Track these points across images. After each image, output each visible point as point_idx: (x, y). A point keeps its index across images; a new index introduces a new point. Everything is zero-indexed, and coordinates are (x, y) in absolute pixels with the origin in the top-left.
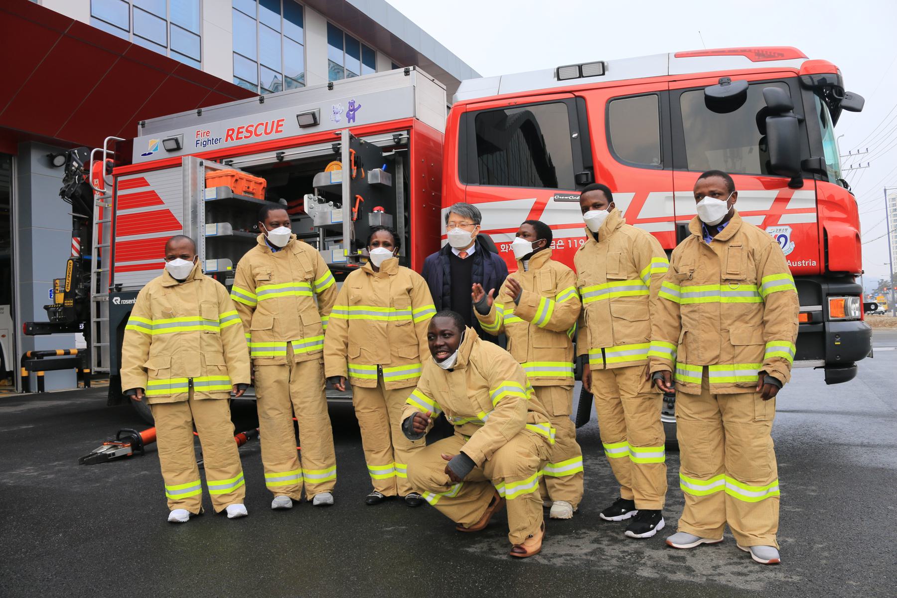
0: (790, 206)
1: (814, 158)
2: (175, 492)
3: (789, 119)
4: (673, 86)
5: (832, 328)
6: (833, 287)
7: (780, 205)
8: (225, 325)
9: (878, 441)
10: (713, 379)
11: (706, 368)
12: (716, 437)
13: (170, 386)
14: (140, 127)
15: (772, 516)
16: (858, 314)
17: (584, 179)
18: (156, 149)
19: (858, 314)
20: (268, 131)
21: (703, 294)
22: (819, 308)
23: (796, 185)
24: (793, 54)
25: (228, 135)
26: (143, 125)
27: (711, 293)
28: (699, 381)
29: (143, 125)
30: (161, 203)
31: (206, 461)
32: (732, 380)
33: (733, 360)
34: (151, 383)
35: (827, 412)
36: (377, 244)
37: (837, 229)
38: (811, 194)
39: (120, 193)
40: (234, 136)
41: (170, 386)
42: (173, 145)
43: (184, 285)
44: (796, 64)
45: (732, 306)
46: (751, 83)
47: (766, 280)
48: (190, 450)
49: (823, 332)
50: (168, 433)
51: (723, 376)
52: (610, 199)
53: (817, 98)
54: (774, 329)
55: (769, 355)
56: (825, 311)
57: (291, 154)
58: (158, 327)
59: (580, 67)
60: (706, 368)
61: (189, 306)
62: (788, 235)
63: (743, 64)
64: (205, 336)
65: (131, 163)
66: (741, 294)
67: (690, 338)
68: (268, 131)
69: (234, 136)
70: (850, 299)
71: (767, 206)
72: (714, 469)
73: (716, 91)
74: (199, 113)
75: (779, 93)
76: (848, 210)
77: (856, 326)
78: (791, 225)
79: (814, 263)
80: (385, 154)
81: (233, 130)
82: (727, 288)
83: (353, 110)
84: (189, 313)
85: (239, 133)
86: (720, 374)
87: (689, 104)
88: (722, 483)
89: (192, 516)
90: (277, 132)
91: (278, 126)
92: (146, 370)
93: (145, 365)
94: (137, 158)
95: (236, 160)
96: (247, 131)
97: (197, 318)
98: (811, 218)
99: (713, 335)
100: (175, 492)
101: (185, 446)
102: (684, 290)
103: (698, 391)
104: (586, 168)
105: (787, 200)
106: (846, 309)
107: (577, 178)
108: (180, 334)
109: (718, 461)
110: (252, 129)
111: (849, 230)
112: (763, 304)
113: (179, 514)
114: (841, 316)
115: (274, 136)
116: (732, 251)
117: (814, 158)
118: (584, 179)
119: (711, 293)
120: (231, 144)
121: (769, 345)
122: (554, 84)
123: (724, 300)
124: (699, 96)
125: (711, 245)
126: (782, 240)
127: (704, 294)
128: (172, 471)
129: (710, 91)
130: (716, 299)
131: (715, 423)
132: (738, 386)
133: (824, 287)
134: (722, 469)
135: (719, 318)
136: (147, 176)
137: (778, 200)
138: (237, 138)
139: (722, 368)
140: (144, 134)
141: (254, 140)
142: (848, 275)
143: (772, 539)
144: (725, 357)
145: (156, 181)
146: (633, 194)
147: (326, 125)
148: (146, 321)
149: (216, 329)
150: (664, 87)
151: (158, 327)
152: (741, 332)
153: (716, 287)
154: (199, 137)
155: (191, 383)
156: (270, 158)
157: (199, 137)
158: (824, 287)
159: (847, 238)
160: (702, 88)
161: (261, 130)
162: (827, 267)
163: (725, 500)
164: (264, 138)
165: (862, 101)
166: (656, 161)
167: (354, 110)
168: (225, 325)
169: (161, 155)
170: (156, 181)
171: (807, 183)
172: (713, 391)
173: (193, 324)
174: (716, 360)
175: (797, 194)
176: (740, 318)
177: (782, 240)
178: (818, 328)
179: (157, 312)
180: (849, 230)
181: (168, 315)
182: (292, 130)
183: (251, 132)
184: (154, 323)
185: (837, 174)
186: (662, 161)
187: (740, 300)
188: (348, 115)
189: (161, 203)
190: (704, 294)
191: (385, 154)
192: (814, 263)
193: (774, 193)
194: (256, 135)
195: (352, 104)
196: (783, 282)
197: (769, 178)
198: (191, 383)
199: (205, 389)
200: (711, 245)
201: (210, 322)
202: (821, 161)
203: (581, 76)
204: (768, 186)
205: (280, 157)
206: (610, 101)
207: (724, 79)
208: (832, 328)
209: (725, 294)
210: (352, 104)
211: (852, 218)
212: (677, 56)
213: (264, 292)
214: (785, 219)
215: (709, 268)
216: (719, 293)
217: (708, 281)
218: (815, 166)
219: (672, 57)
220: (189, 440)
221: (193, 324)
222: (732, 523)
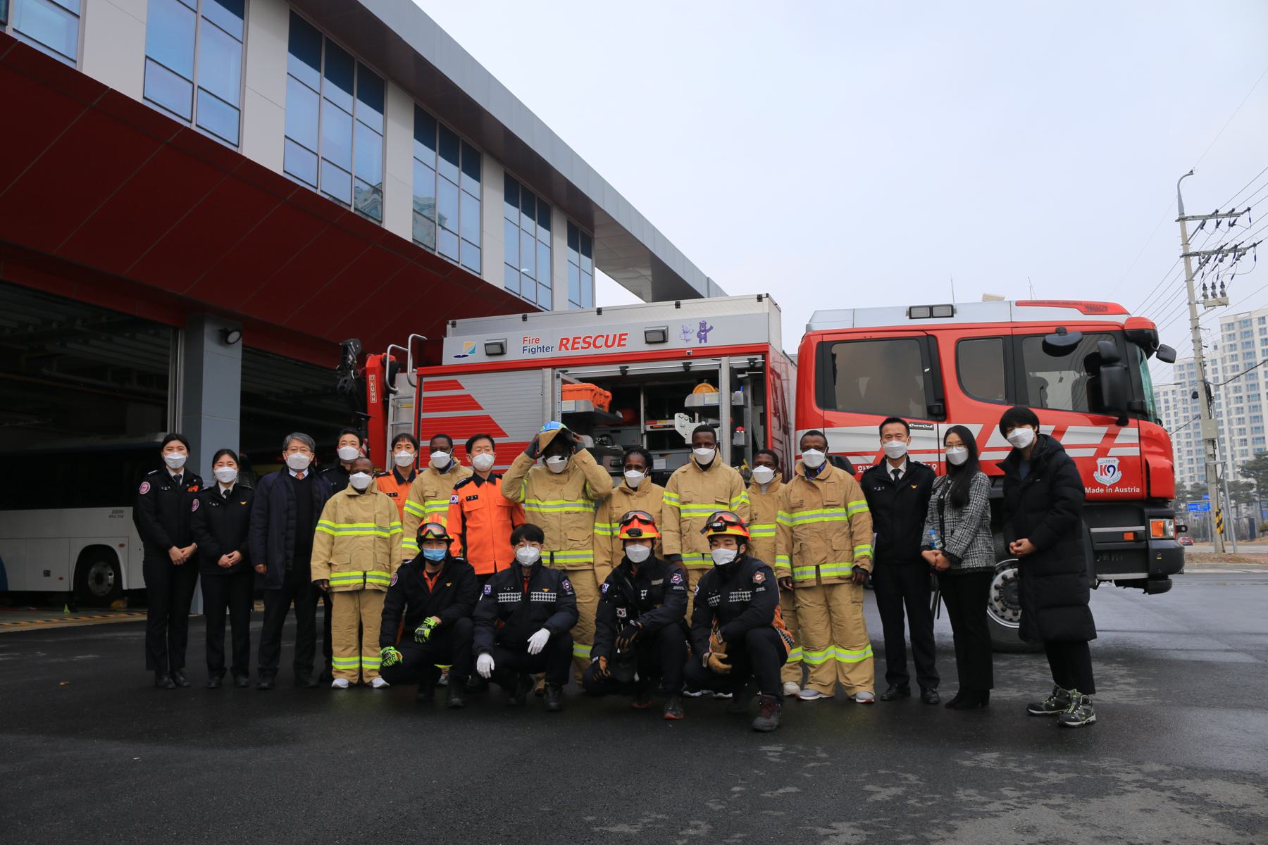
0: (1117, 441)
2: (339, 663)
3: (1117, 368)
4: (1016, 331)
5: (1154, 545)
6: (1154, 510)
7: (1109, 440)
8: (393, 532)
11: (817, 567)
13: (349, 578)
14: (449, 327)
16: (1172, 534)
18: (473, 352)
19: (1172, 534)
20: (610, 343)
21: (809, 517)
23: (1123, 423)
24: (1119, 310)
25: (561, 344)
26: (454, 325)
27: (817, 516)
28: (814, 576)
29: (454, 325)
30: (480, 408)
31: (365, 639)
33: (835, 560)
34: (334, 575)
37: (1156, 461)
38: (1135, 431)
39: (425, 394)
40: (569, 346)
41: (349, 578)
43: (364, 496)
44: (1121, 319)
45: (831, 523)
46: (1084, 333)
47: (851, 505)
50: (342, 615)
52: (908, 433)
56: (1147, 531)
57: (635, 369)
58: (339, 530)
59: (931, 308)
60: (817, 567)
61: (366, 515)
63: (1075, 316)
64: (379, 543)
67: (805, 548)
68: (610, 343)
69: (569, 346)
70: (1167, 521)
72: (826, 642)
73: (1054, 340)
74: (525, 319)
75: (1107, 344)
76: (1161, 443)
77: (1172, 544)
78: (1119, 457)
79: (1138, 490)
82: (828, 511)
84: (366, 521)
85: (574, 343)
86: (827, 570)
88: (833, 652)
91: (620, 339)
92: (330, 565)
93: (331, 561)
94: (448, 359)
95: (571, 371)
96: (584, 341)
97: (372, 525)
98: (1135, 452)
99: (821, 544)
100: (339, 663)
101: (351, 627)
102: (796, 515)
103: (814, 583)
106: (1164, 530)
108: (358, 536)
110: (591, 341)
111: (1165, 462)
112: (850, 521)
113: (340, 682)
114: (1161, 536)
115: (616, 350)
117: (1137, 401)
119: (817, 516)
120: (564, 353)
122: (906, 322)
123: (826, 519)
126: (1111, 469)
127: (812, 516)
128: (340, 646)
130: (821, 519)
131: (824, 609)
133: (1147, 510)
134: (832, 642)
135: (821, 531)
136: (461, 379)
137: (1107, 435)
138: (573, 348)
139: (828, 566)
140: (454, 335)
141: (592, 351)
142: (1162, 502)
144: (830, 558)
145: (471, 385)
146: (981, 426)
147: (674, 343)
148: (332, 524)
149: (386, 535)
150: (1008, 332)
151: (339, 530)
152: (839, 541)
153: (820, 511)
154: (527, 344)
155: (365, 576)
156: (614, 370)
157: (527, 344)
158: (1147, 510)
159: (1163, 469)
161: (601, 342)
162: (1149, 493)
164: (604, 351)
168: (393, 532)
169: (480, 357)
170: (471, 385)
171: (1131, 421)
173: (369, 529)
174: (824, 561)
175: (1124, 431)
176: (838, 530)
177: (1111, 469)
178: (1142, 545)
179: (341, 517)
180: (1165, 462)
181: (350, 521)
182: (636, 344)
183: (589, 343)
184: (337, 526)
185: (1155, 414)
187: (837, 518)
188: (699, 335)
189: (480, 408)
190: (812, 516)
192: (1138, 490)
193: (1104, 430)
194: (595, 346)
196: (861, 506)
197: (1094, 416)
198: (365, 576)
201: (381, 528)
202: (1143, 404)
203: (931, 316)
204: (1096, 423)
205: (623, 370)
206: (959, 341)
207: (1061, 329)
208: (1154, 545)
209: (826, 515)
211: (1168, 453)
212: (1019, 304)
213: (430, 506)
214: (1114, 451)
216: (822, 515)
217: (813, 507)
218: (1137, 407)
219: (1013, 304)
220: (355, 623)
221: (369, 529)
222: (842, 680)
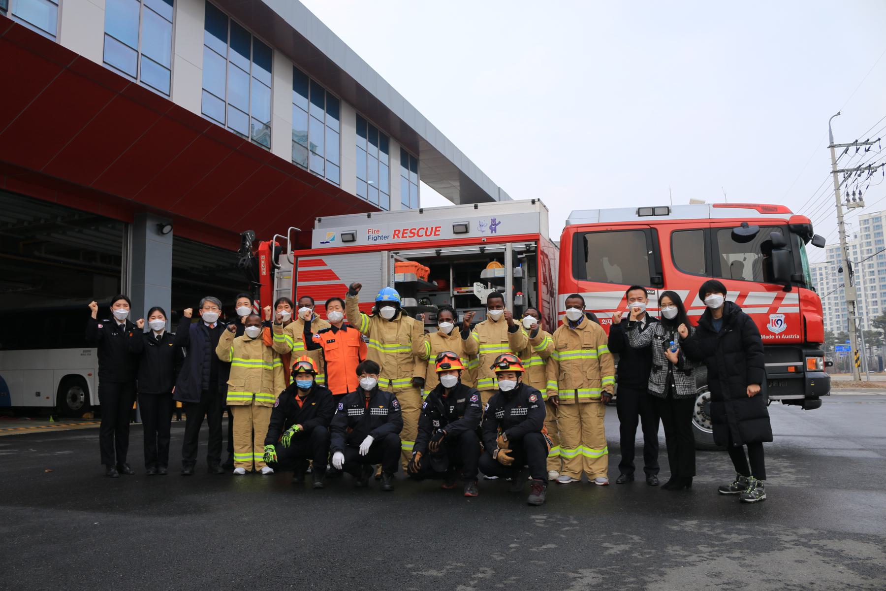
0: (783, 302)
1: (798, 274)
3: (784, 251)
4: (713, 225)
6: (809, 351)
7: (777, 301)
9: (834, 447)
10: (580, 396)
11: (576, 390)
12: (578, 426)
15: (604, 464)
17: (656, 281)
18: (333, 239)
19: (822, 368)
20: (428, 233)
22: (801, 363)
23: (788, 289)
24: (785, 210)
25: (395, 234)
27: (577, 354)
30: (337, 279)
32: (588, 396)
33: (589, 386)
35: (877, 438)
36: (442, 321)
37: (811, 317)
38: (796, 296)
39: (300, 269)
40: (400, 235)
42: (350, 238)
44: (787, 217)
46: (761, 227)
48: (250, 434)
49: (804, 378)
51: (585, 394)
53: (798, 237)
54: (606, 371)
55: (604, 384)
56: (804, 365)
57: (446, 251)
59: (653, 209)
60: (576, 390)
62: (783, 319)
63: (754, 214)
65: (310, 248)
66: (590, 354)
68: (428, 233)
69: (400, 235)
70: (819, 359)
71: (770, 302)
73: (739, 231)
75: (777, 235)
76: (815, 304)
77: (822, 375)
78: (785, 314)
79: (798, 337)
80: (519, 256)
81: (399, 231)
82: (584, 351)
83: (494, 225)
85: (404, 233)
86: (583, 393)
87: (724, 239)
89: (247, 472)
90: (435, 235)
91: (436, 231)
94: (316, 244)
96: (411, 232)
98: (796, 310)
99: (579, 374)
104: (658, 273)
105: (782, 299)
106: (816, 365)
107: (652, 280)
109: (579, 438)
110: (416, 232)
111: (817, 317)
114: (814, 369)
115: (433, 238)
116: (586, 334)
117: (798, 274)
118: (656, 281)
119: (577, 354)
121: (603, 379)
123: (583, 357)
124: (729, 232)
125: (577, 331)
127: (573, 355)
129: (736, 231)
130: (580, 357)
131: (578, 419)
132: (591, 399)
133: (804, 351)
134: (581, 443)
136: (324, 258)
139: (583, 390)
141: (416, 239)
142: (815, 345)
143: (604, 475)
145: (332, 263)
149: (271, 368)
150: (707, 226)
154: (370, 234)
155: (254, 396)
156: (431, 252)
157: (370, 234)
158: (804, 351)
160: (732, 228)
161: (422, 232)
162: (806, 339)
163: (584, 458)
164: (425, 239)
165: (824, 241)
166: (703, 271)
167: (496, 225)
169: (338, 243)
170: (332, 263)
172: (580, 401)
174: (581, 386)
180: (817, 317)
182: (447, 234)
183: (414, 234)
185: (810, 284)
186: (706, 271)
188: (491, 228)
189: (337, 279)
190: (573, 355)
191: (519, 256)
192: (798, 337)
193: (774, 294)
195: (494, 220)
197: (767, 285)
198: (254, 396)
199: (262, 400)
200: (577, 331)
201: (267, 363)
202: (802, 277)
203: (654, 214)
204: (769, 290)
205: (438, 253)
206: (672, 232)
207: (744, 224)
208: (809, 375)
210: (494, 220)
214: (781, 310)
215: (576, 342)
217: (575, 348)
218: (798, 279)
220: (250, 429)
222: (586, 469)
